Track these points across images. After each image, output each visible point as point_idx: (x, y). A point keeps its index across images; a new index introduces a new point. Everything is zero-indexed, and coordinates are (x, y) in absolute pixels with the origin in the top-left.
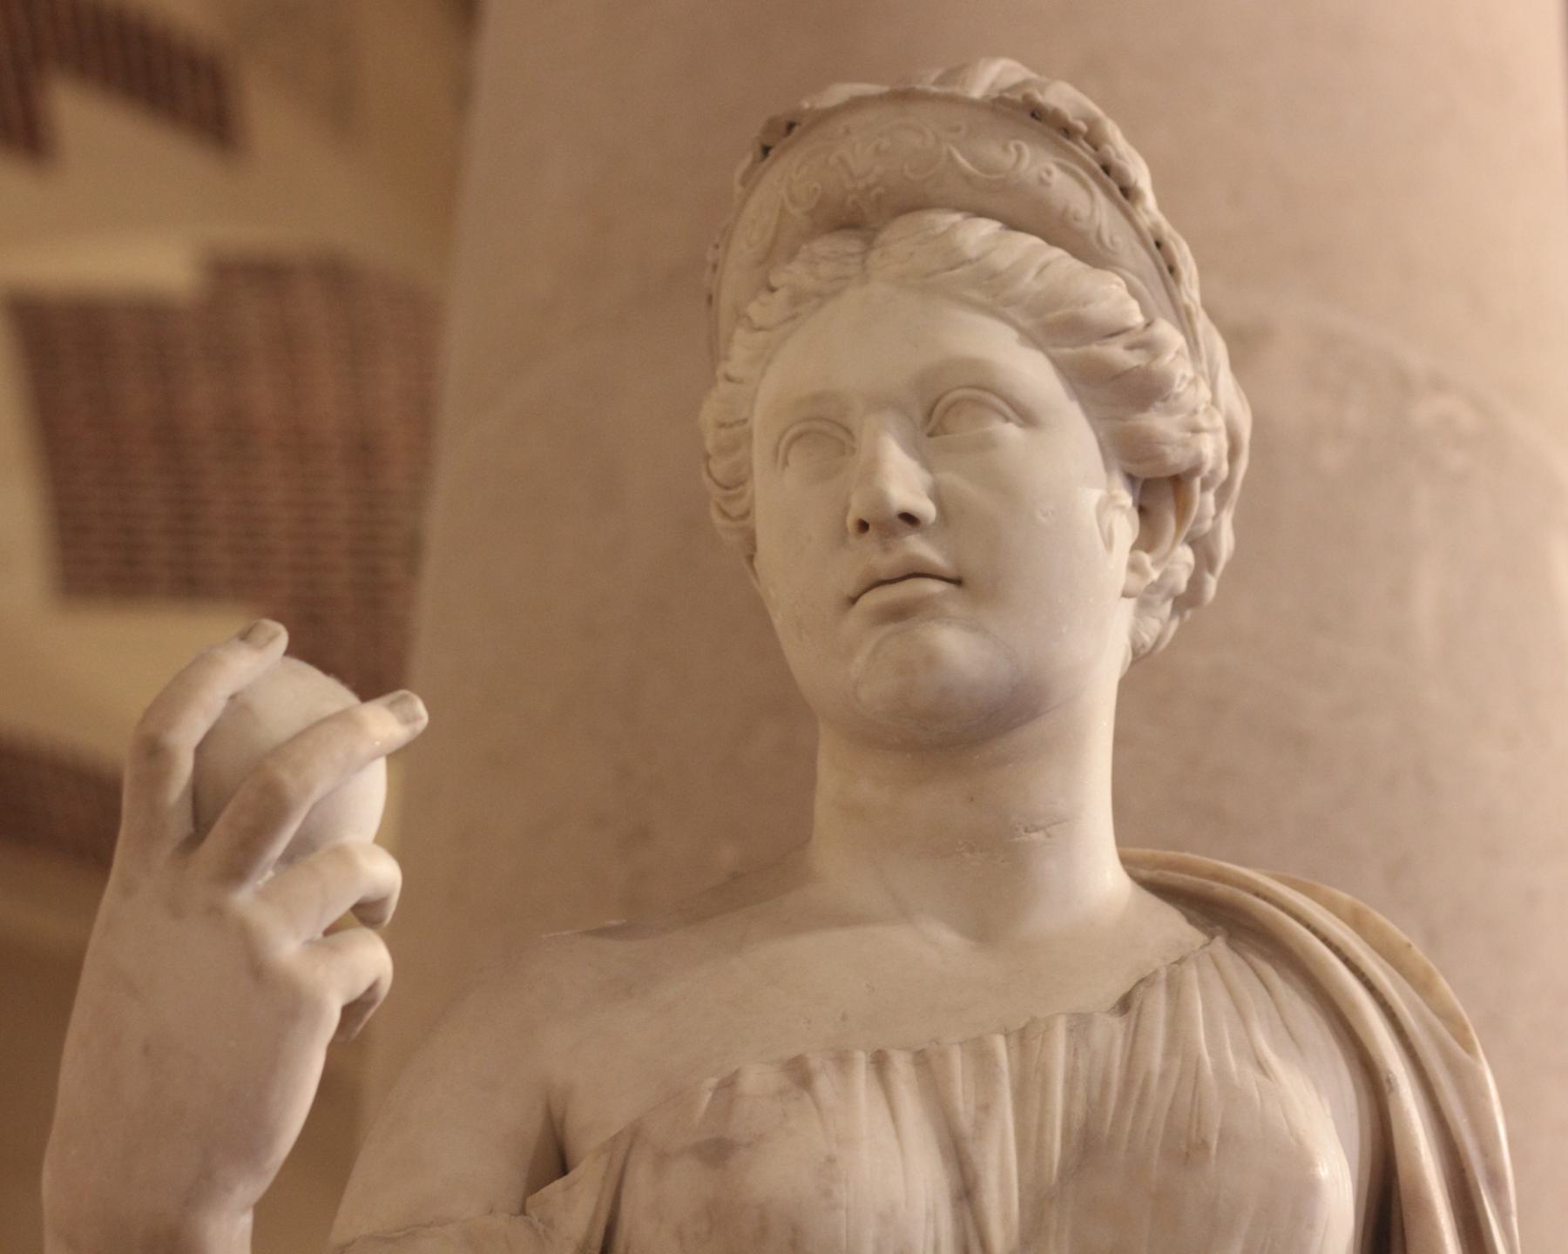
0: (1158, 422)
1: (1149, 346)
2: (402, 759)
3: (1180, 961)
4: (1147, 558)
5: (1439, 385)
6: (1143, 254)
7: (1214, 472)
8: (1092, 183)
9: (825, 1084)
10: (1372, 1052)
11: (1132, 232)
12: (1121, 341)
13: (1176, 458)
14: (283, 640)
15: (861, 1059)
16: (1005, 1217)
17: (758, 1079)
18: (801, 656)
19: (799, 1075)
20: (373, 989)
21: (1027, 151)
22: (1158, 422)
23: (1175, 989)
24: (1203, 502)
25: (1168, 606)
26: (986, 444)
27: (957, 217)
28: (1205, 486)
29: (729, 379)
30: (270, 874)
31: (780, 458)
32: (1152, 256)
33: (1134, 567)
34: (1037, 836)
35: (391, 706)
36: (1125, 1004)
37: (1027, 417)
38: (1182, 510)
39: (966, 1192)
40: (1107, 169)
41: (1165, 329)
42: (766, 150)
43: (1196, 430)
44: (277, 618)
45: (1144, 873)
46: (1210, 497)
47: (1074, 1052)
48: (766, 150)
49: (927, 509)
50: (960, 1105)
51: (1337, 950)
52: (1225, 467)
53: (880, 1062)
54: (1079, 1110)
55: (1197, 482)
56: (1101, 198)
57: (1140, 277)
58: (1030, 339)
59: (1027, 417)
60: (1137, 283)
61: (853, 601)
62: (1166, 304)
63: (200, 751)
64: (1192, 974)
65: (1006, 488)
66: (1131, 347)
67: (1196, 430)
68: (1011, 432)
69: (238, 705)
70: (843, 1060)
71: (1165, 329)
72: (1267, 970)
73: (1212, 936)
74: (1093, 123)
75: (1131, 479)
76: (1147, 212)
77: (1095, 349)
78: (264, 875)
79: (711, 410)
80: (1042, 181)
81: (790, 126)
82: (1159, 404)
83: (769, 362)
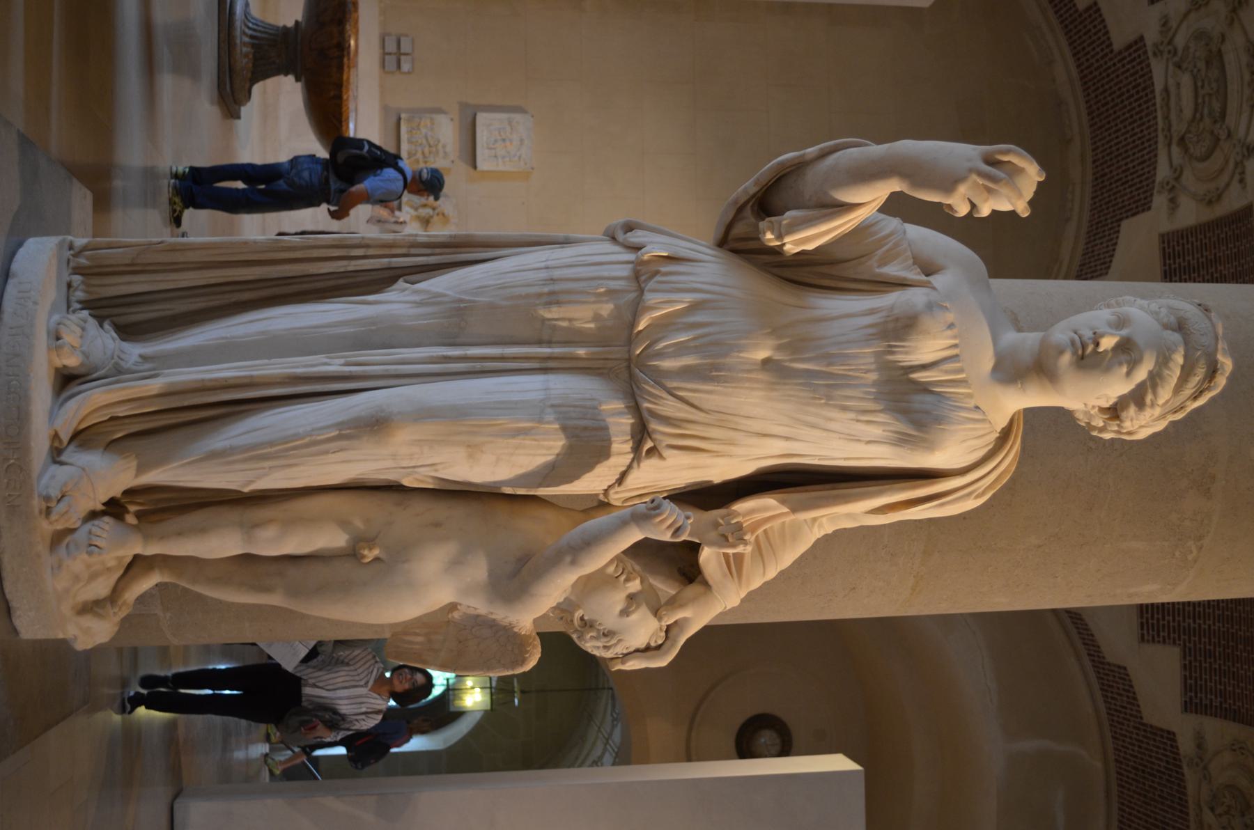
0: (1132, 410)
1: (1153, 405)
2: (1013, 214)
3: (990, 422)
4: (1097, 409)
5: (1200, 548)
6: (1178, 404)
7: (1122, 427)
8: (1196, 388)
9: (949, 332)
10: (972, 472)
11: (1185, 399)
12: (1153, 398)
13: (1124, 415)
14: (1041, 180)
15: (956, 341)
16: (923, 377)
17: (950, 317)
18: (1062, 324)
19: (951, 326)
20: (956, 212)
21: (1203, 370)
22: (1132, 410)
23: (983, 421)
24: (1114, 426)
25: (1087, 421)
26: (1120, 364)
27: (1183, 353)
28: (1119, 425)
29: (1135, 300)
30: (981, 183)
31: (1113, 314)
32: (1178, 406)
33: (1094, 407)
34: (1020, 386)
35: (1025, 207)
36: (977, 407)
37: (1128, 374)
38: (1111, 419)
39: (924, 367)
40: (1201, 392)
41: (1158, 411)
42: (1200, 305)
43: (1132, 420)
44: (1046, 177)
45: (1016, 418)
46: (1116, 428)
47: (963, 394)
48: (1200, 305)
49: (1101, 349)
50: (947, 366)
51: (1000, 462)
52: (1125, 431)
53: (955, 346)
54: (948, 395)
55: (1118, 422)
56: (1192, 391)
57: (1172, 403)
58: (1150, 373)
59: (1128, 374)
60: (1171, 402)
61: (1076, 333)
62: (1167, 411)
63: (1009, 162)
64: (987, 425)
65: (1108, 369)
66: (1151, 400)
67: (1132, 420)
68: (1124, 369)
69: (1021, 171)
70: (955, 337)
71: (1158, 411)
72: (990, 447)
73: (1000, 433)
74: (1215, 387)
75: (1116, 404)
76: (1191, 404)
77: (1150, 390)
78: (981, 181)
79: (1127, 298)
80: (1195, 375)
81: (1206, 310)
82: (1137, 409)
83: (1140, 309)
